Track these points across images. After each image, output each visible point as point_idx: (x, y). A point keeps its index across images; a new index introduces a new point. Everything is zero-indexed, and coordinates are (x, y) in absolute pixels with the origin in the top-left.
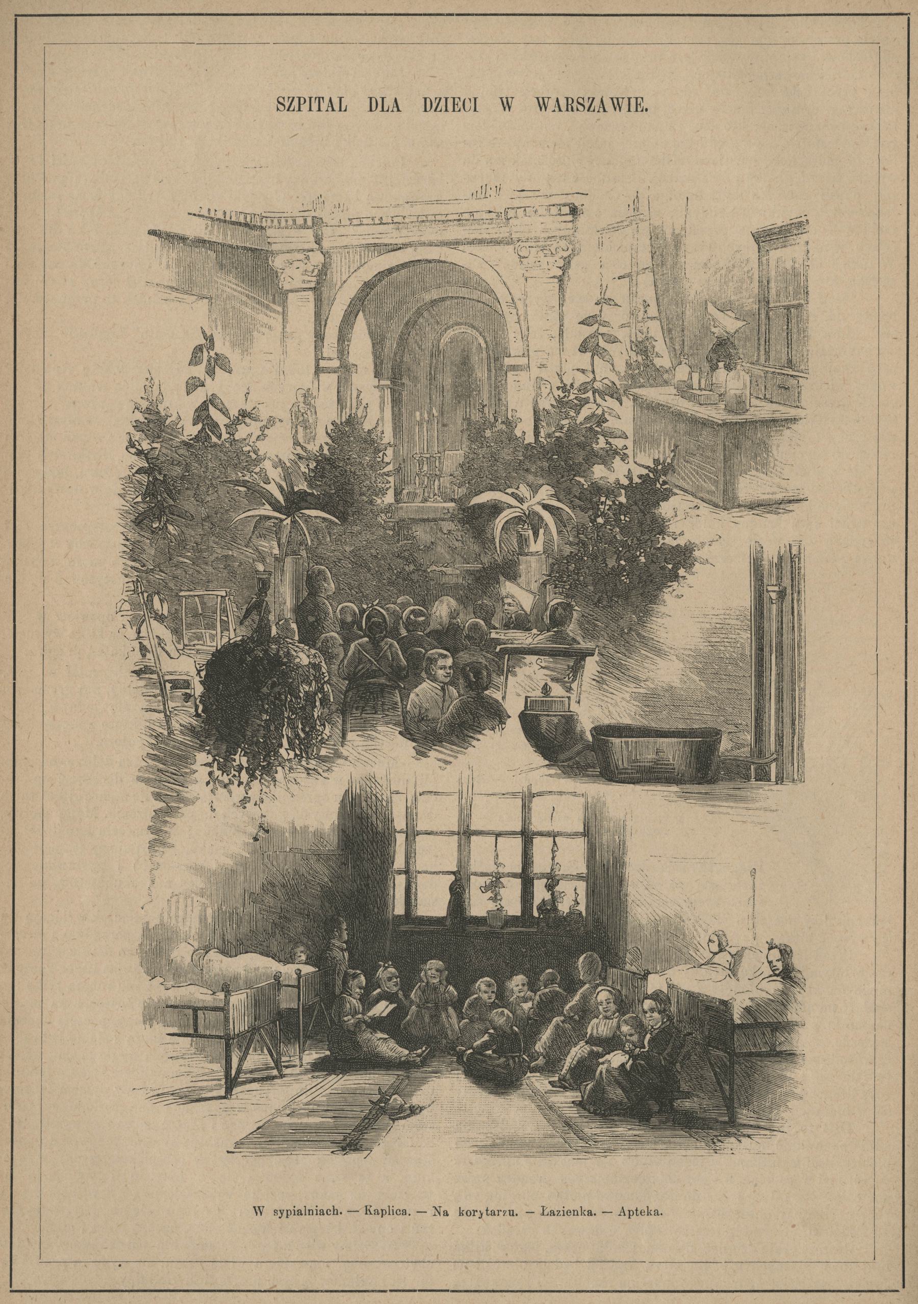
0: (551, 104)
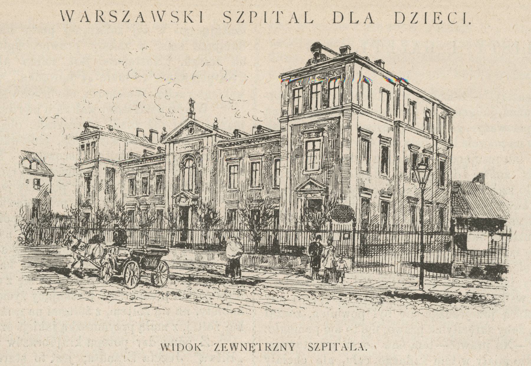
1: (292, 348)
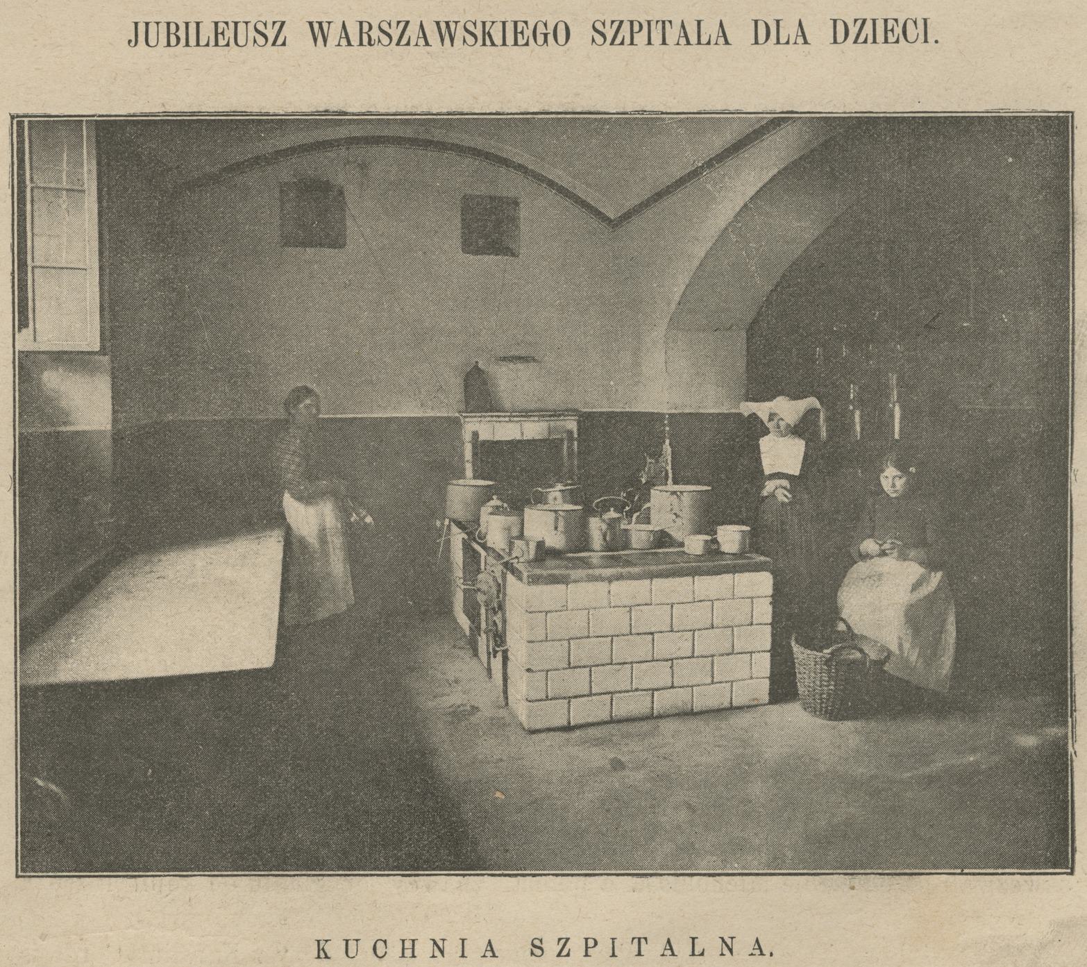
0: (334, 34)
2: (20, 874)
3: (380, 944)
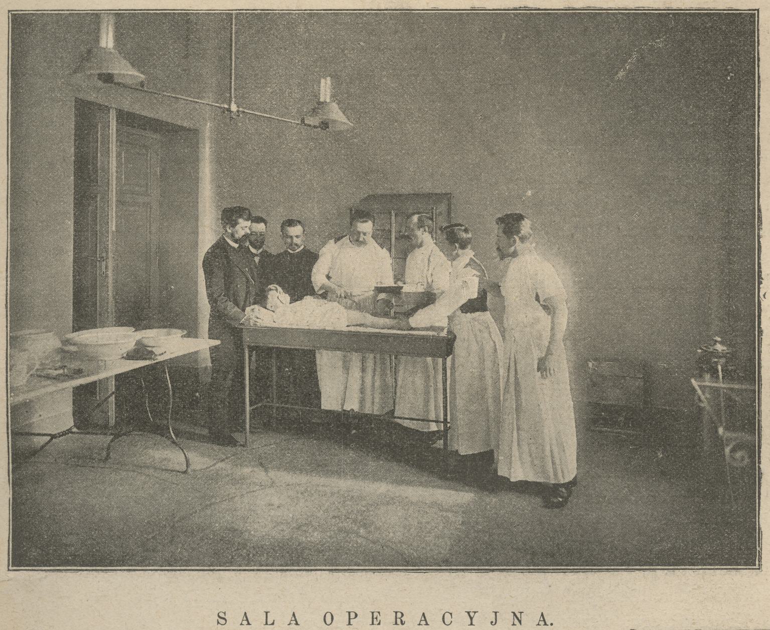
1: (471, 618)
2: (11, 568)
3: (447, 615)
